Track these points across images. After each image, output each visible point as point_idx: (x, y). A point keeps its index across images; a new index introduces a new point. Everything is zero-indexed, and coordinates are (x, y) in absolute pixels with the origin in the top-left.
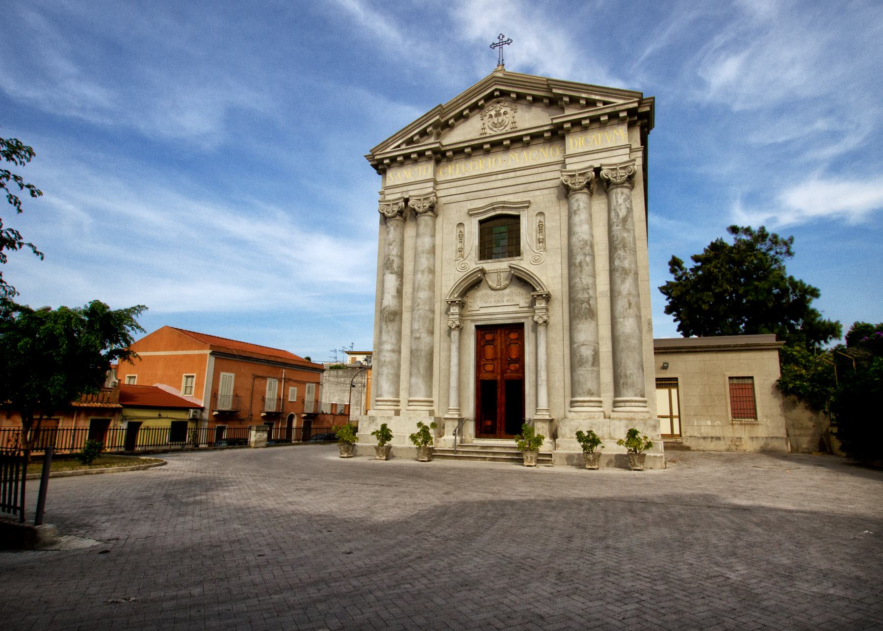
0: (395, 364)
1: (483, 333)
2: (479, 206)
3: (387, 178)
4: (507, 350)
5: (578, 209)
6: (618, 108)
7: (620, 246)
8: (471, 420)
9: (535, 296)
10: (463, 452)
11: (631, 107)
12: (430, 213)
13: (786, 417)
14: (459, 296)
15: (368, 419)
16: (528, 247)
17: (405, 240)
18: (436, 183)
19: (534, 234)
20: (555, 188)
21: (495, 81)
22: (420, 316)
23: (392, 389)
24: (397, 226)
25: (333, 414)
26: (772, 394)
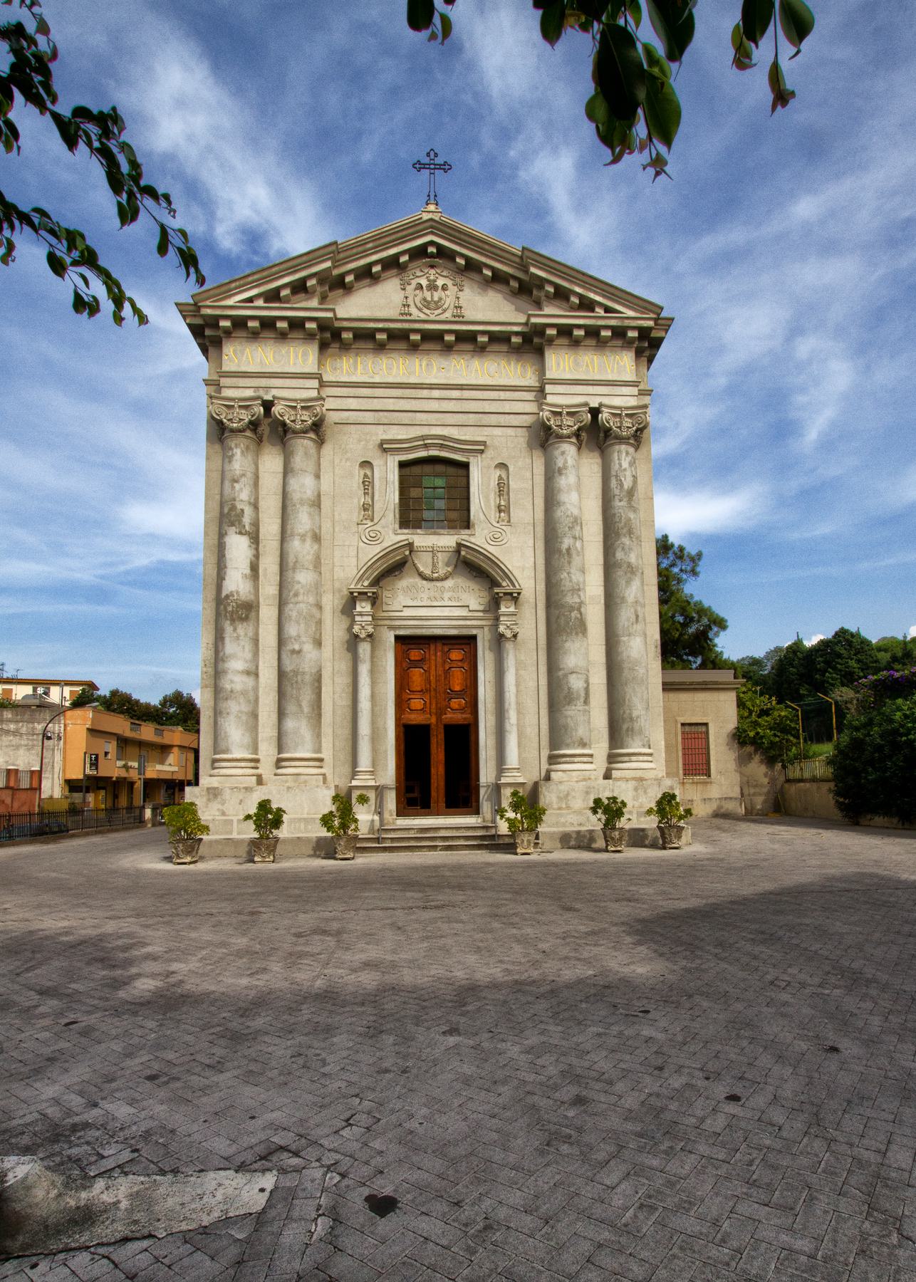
0: (251, 696)
1: (446, 649)
2: (399, 437)
3: (225, 357)
4: (445, 678)
5: (565, 468)
6: (627, 323)
7: (625, 531)
8: (390, 789)
9: (355, 594)
10: (392, 839)
11: (645, 325)
12: (312, 435)
13: (741, 773)
14: (372, 585)
15: (204, 793)
16: (481, 514)
17: (260, 475)
18: (323, 384)
19: (492, 496)
20: (525, 429)
21: (432, 227)
22: (300, 613)
23: (247, 740)
24: (247, 448)
25: (12, 788)
26: (727, 745)
